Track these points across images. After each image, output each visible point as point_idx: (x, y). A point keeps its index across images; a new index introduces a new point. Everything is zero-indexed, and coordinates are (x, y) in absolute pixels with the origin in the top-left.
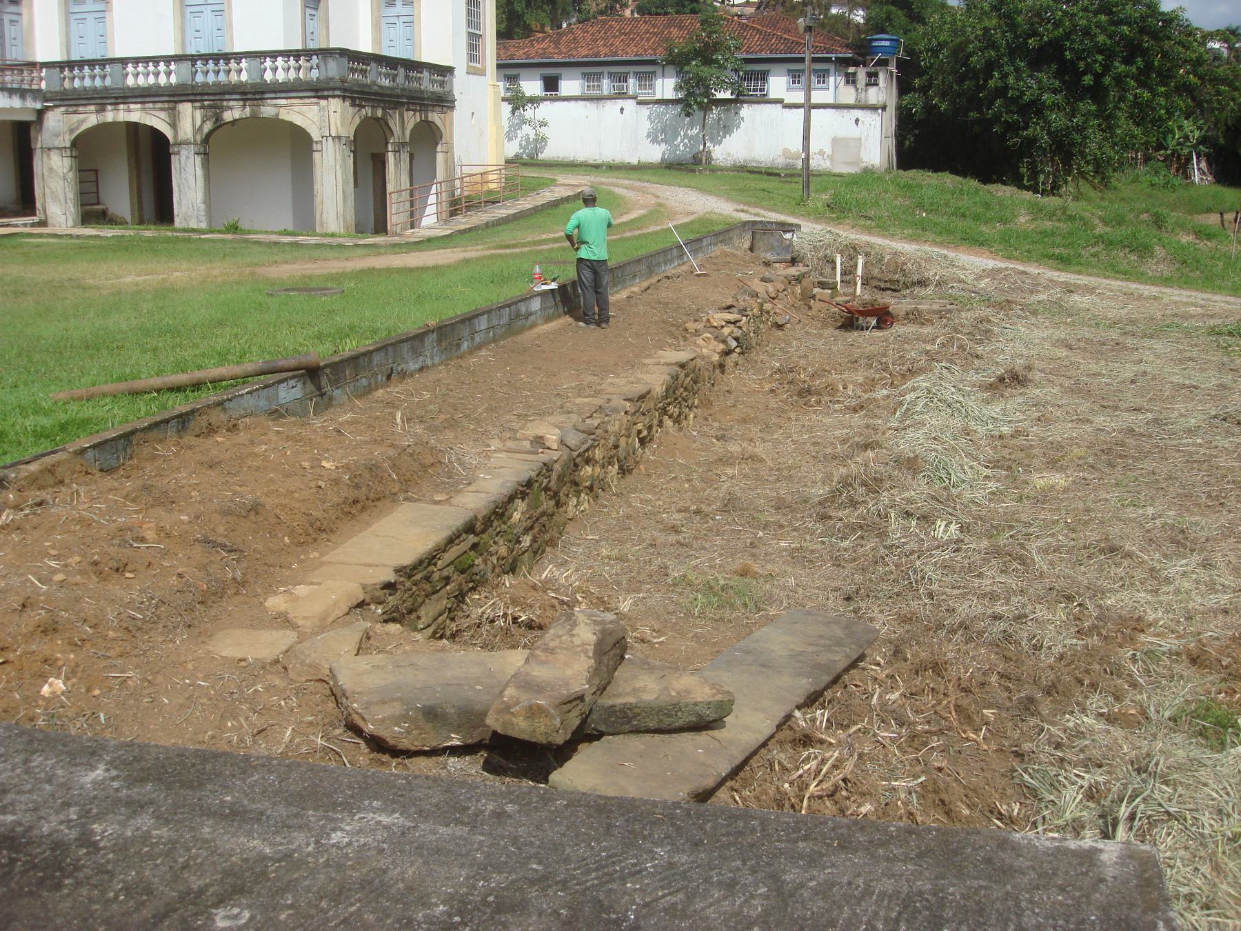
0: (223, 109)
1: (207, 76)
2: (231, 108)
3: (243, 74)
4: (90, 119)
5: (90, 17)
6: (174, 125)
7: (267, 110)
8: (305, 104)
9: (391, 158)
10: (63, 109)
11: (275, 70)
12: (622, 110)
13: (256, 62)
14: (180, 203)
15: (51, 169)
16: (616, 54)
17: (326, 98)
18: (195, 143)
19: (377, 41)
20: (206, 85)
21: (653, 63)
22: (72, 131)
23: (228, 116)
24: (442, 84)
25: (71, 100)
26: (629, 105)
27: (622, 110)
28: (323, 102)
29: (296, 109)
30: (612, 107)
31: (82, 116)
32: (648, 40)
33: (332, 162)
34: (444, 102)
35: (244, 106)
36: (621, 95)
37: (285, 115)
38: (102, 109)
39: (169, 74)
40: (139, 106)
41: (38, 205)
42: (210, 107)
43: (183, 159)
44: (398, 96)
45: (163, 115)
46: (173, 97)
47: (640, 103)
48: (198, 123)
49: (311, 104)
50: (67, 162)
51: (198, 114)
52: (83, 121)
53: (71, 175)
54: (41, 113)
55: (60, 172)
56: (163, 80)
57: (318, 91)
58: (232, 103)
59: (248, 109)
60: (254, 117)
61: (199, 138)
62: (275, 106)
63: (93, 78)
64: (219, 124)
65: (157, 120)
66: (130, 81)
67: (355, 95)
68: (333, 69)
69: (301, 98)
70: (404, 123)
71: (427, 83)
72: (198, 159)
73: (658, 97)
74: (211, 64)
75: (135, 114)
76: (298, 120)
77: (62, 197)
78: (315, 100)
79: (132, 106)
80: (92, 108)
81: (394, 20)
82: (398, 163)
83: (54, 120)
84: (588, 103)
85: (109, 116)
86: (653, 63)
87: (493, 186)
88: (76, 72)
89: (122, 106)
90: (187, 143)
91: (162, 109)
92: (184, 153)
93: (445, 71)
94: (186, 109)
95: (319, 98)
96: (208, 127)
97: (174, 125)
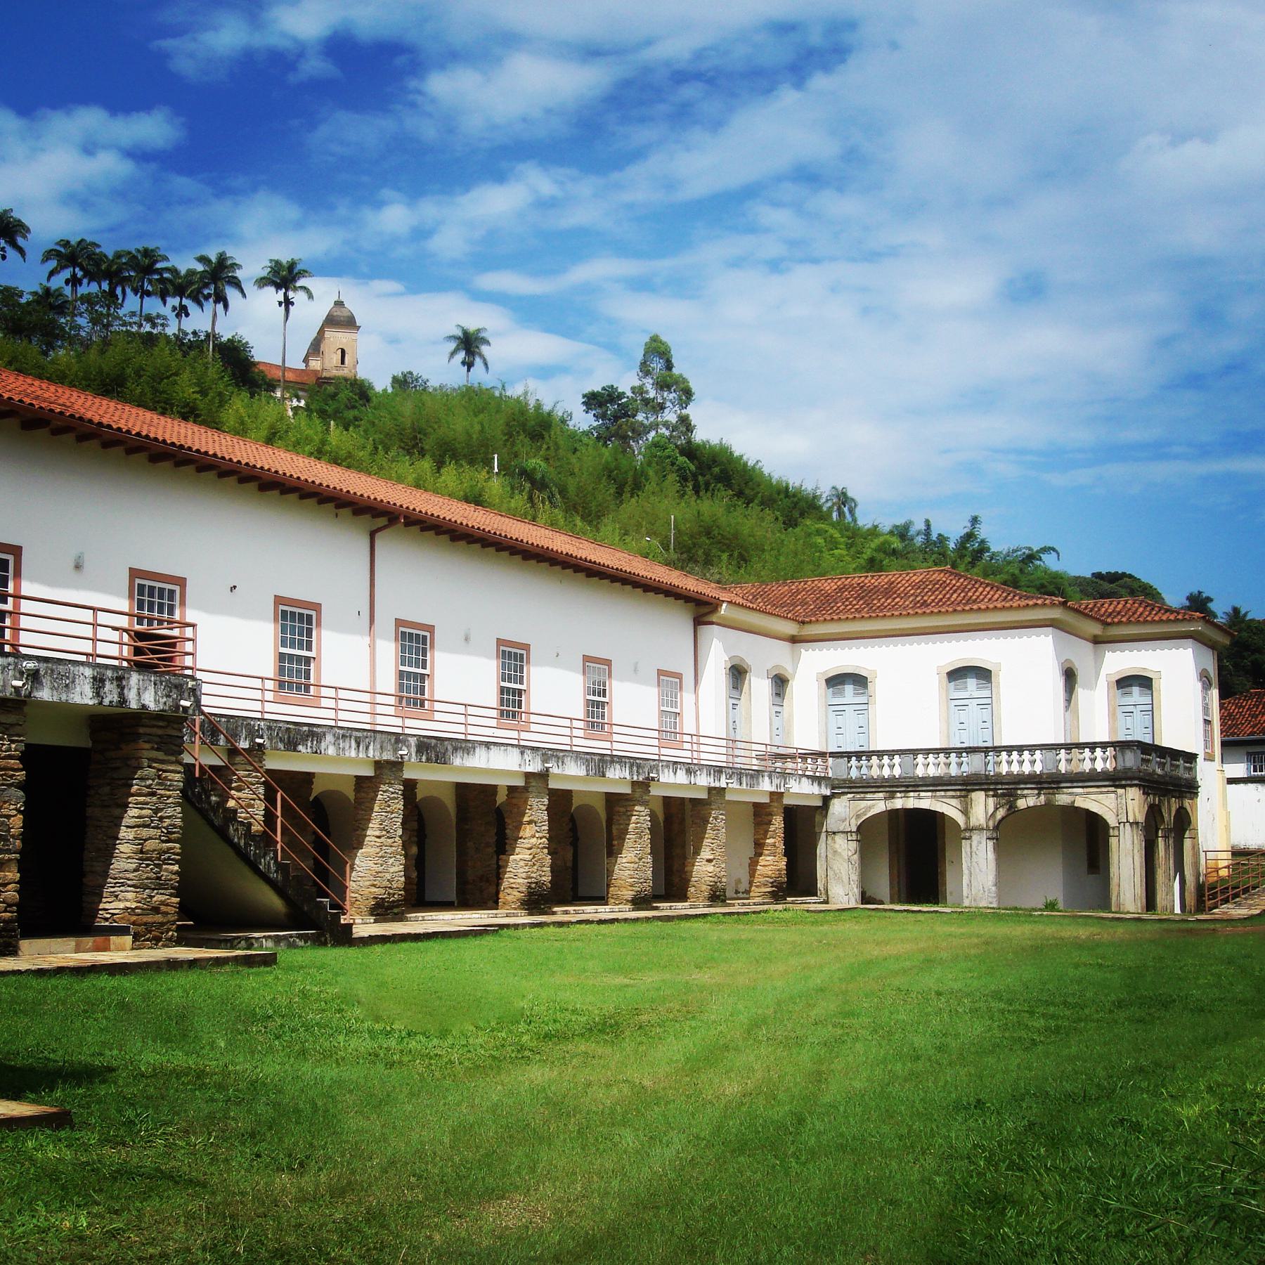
0: (1017, 797)
3: (1034, 765)
4: (878, 805)
6: (965, 812)
7: (1063, 799)
8: (1101, 793)
14: (970, 885)
18: (988, 829)
20: (1009, 774)
22: (858, 816)
23: (1022, 804)
28: (1120, 791)
29: (1093, 797)
34: (1190, 788)
35: (1039, 794)
37: (1081, 803)
38: (891, 796)
42: (1003, 795)
43: (974, 843)
45: (954, 802)
46: (966, 786)
48: (991, 810)
49: (1108, 792)
50: (853, 845)
52: (870, 807)
53: (856, 857)
54: (826, 800)
57: (1115, 780)
59: (1042, 797)
60: (1049, 804)
61: (991, 824)
62: (1071, 794)
65: (947, 806)
67: (1149, 785)
72: (990, 843)
75: (925, 802)
76: (1094, 808)
77: (846, 881)
80: (881, 795)
84: (1251, 786)
90: (980, 829)
91: (953, 797)
92: (976, 837)
94: (979, 797)
95: (1117, 787)
96: (1001, 813)
97: (965, 812)
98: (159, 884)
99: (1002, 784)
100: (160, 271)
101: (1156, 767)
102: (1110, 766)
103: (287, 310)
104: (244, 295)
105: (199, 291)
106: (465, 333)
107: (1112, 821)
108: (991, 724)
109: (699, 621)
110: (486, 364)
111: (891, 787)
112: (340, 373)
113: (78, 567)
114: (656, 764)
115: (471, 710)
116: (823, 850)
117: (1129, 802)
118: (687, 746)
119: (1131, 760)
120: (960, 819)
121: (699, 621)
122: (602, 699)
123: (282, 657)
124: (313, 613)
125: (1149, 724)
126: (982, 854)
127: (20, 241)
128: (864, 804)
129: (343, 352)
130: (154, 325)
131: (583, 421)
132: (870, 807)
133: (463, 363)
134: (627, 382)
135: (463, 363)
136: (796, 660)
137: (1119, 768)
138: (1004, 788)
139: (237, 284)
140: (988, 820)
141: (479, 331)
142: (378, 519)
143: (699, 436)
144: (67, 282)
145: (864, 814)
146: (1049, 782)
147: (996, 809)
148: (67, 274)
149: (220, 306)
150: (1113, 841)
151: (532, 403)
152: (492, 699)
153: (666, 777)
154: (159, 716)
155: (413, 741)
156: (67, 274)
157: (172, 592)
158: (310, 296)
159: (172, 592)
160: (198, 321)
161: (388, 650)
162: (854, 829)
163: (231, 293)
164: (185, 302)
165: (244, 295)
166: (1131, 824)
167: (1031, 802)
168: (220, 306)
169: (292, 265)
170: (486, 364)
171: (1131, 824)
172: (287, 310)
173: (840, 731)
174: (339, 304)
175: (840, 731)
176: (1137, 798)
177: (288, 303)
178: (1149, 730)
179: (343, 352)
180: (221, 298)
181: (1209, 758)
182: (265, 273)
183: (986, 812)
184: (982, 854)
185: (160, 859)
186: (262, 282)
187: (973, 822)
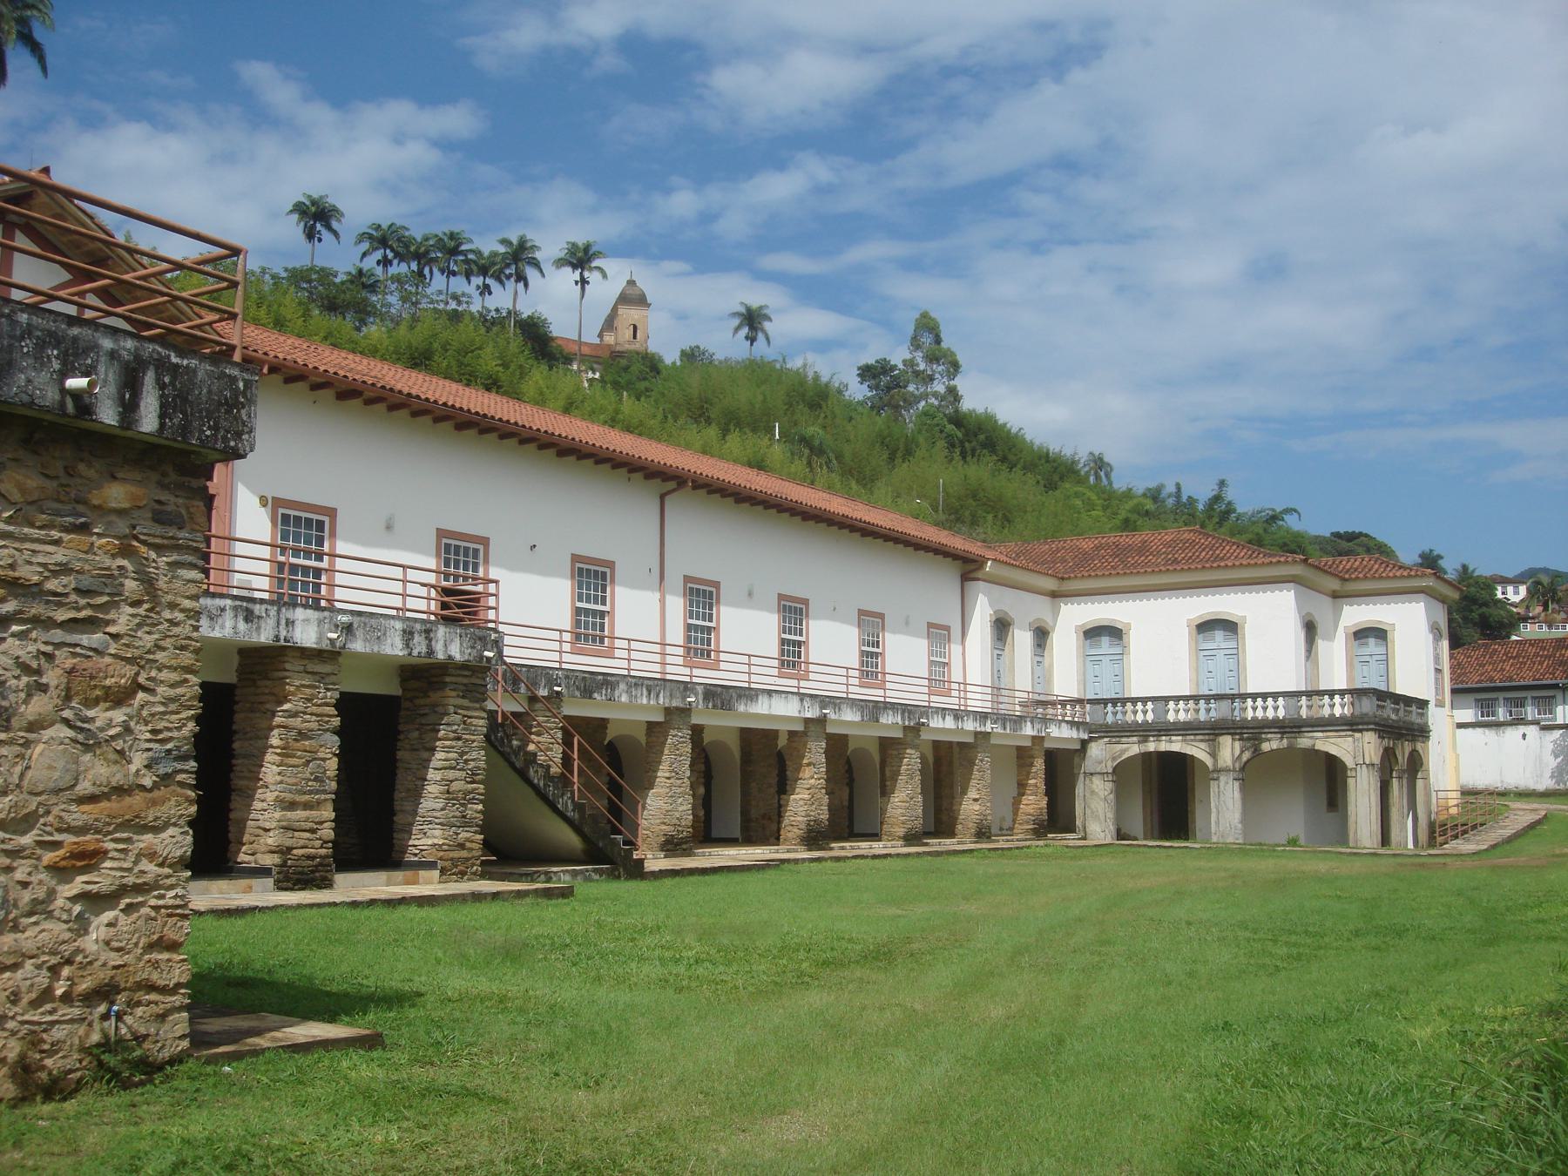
0: (1263, 741)
4: (1133, 748)
7: (1304, 742)
9: (1395, 782)
12: (1524, 736)
13: (1293, 701)
14: (1218, 823)
15: (1093, 792)
16: (1511, 679)
17: (1360, 731)
19: (1350, 678)
20: (1254, 719)
21: (1555, 687)
22: (1114, 759)
23: (1266, 747)
24: (1422, 715)
26: (1532, 731)
27: (1524, 736)
28: (1357, 735)
30: (1513, 734)
32: (1541, 663)
33: (1365, 783)
34: (1422, 733)
36: (1519, 721)
37: (1322, 746)
38: (1145, 740)
41: (1078, 823)
44: (1400, 728)
45: (1203, 745)
46: (1213, 731)
47: (1544, 728)
48: (1237, 752)
50: (1110, 785)
54: (1084, 743)
55: (1102, 794)
57: (1352, 725)
60: (1290, 748)
61: (1237, 766)
63: (1187, 711)
64: (1257, 752)
65: (1197, 750)
66: (1171, 717)
68: (1368, 706)
70: (1403, 750)
72: (1237, 784)
73: (1560, 721)
74: (1259, 701)
75: (1176, 745)
76: (1333, 751)
82: (1401, 787)
83: (1096, 750)
84: (1479, 730)
85: (1151, 746)
86: (1555, 687)
87: (1454, 811)
88: (1119, 708)
90: (1227, 770)
92: (1223, 779)
93: (1423, 704)
96: (1246, 756)
98: (465, 822)
100: (464, 253)
101: (1390, 713)
103: (583, 289)
105: (501, 271)
106: (749, 310)
107: (1349, 763)
109: (966, 578)
110: (768, 339)
112: (632, 347)
114: (926, 711)
115: (634, 645)
120: (1208, 761)
121: (966, 578)
124: (326, 519)
125: (1383, 672)
127: (335, 224)
129: (635, 328)
130: (459, 303)
131: (858, 391)
133: (747, 338)
134: (898, 356)
135: (747, 338)
136: (1056, 613)
138: (1251, 732)
139: (536, 264)
140: (1234, 762)
141: (761, 308)
142: (668, 482)
143: (967, 405)
144: (379, 263)
148: (378, 255)
149: (521, 285)
151: (811, 375)
153: (936, 723)
154: (464, 666)
155: (700, 689)
156: (378, 255)
157: (604, 574)
158: (605, 276)
159: (476, 551)
160: (501, 298)
161: (676, 605)
163: (531, 273)
164: (488, 281)
167: (1275, 745)
168: (521, 285)
169: (587, 248)
170: (768, 339)
172: (583, 289)
174: (631, 283)
177: (583, 282)
179: (635, 328)
180: (521, 278)
181: (1440, 704)
182: (562, 254)
185: (465, 799)
186: (560, 263)
187: (1221, 764)
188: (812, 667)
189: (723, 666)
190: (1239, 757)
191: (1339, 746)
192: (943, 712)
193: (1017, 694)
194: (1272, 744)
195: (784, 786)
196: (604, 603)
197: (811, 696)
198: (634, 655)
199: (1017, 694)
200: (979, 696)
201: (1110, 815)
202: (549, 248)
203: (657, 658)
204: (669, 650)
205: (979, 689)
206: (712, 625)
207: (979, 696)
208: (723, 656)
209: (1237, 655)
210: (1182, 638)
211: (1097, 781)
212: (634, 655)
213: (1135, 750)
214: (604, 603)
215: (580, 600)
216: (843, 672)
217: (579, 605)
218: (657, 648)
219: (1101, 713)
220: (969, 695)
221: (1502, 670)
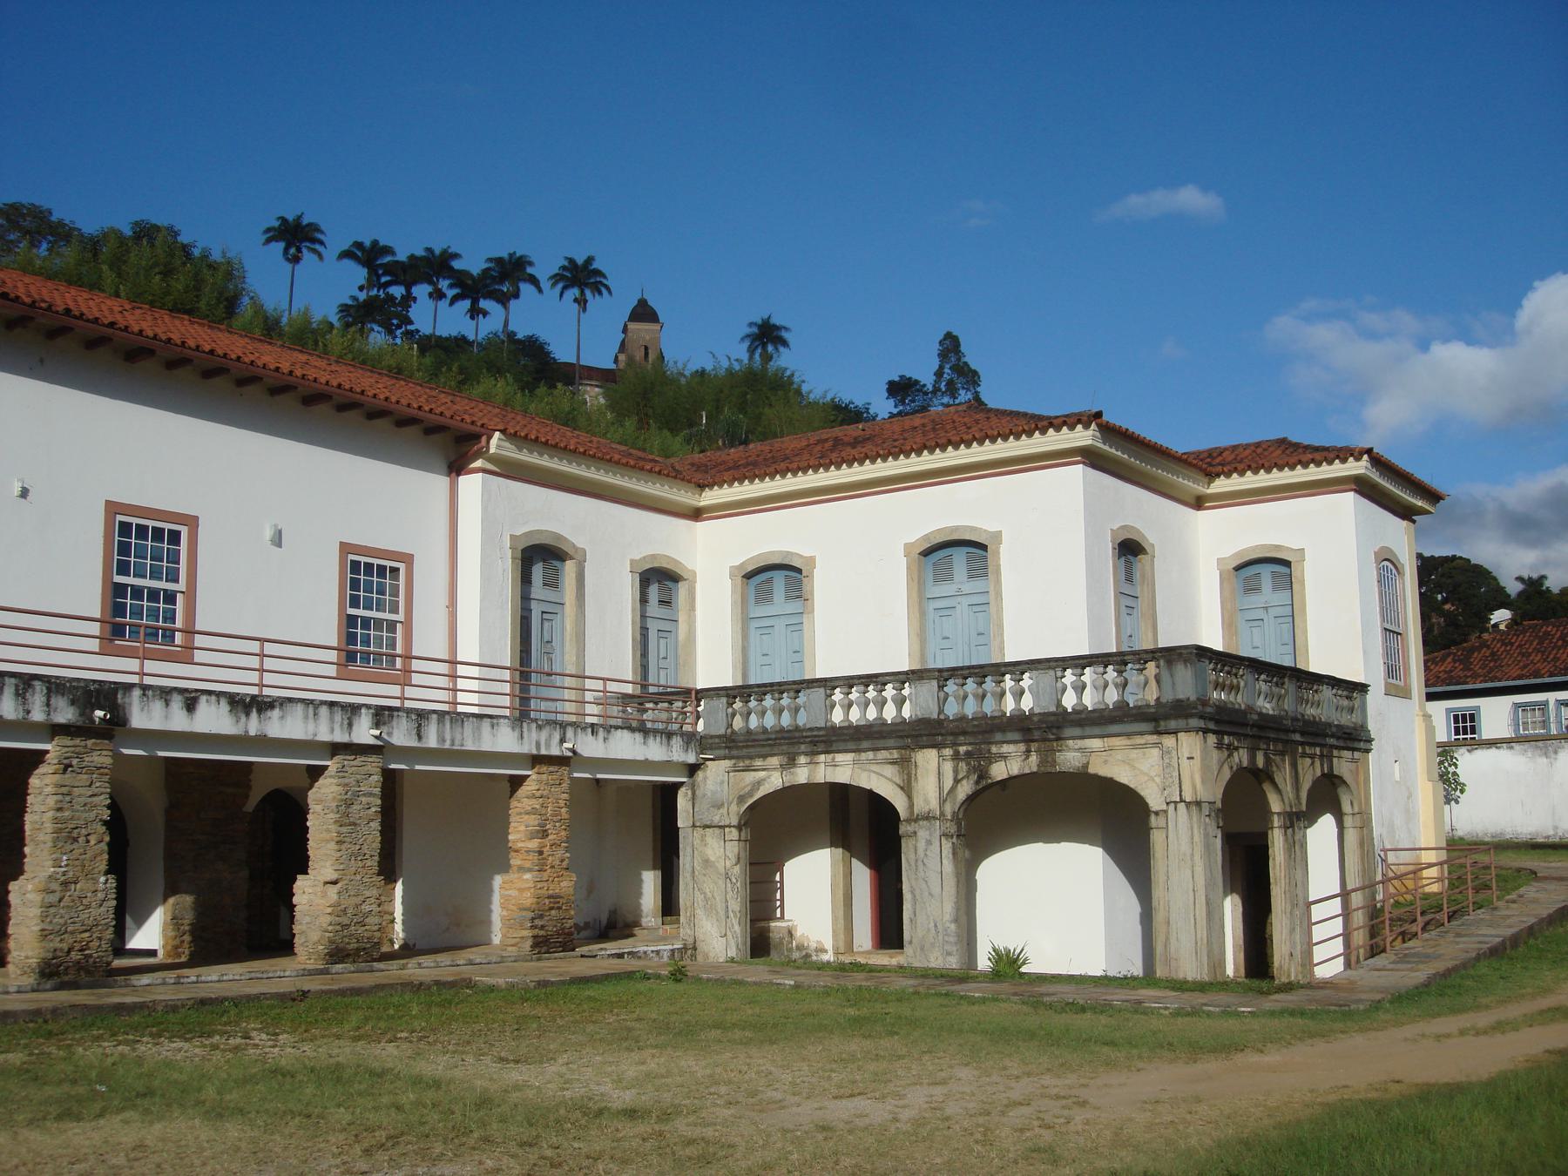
0: (992, 759)
1: (963, 703)
2: (1004, 757)
3: (1022, 698)
4: (771, 778)
5: (780, 624)
6: (907, 789)
7: (1070, 756)
8: (1135, 747)
10: (727, 763)
11: (1080, 688)
20: (962, 718)
22: (741, 799)
23: (999, 771)
25: (740, 747)
28: (1169, 741)
29: (1119, 756)
31: (762, 774)
33: (1185, 847)
34: (1356, 739)
39: (900, 702)
40: (850, 757)
43: (921, 845)
45: (890, 771)
46: (909, 737)
48: (948, 783)
49: (1144, 746)
50: (733, 849)
51: (948, 767)
52: (759, 783)
53: (737, 869)
56: (890, 713)
57: (1158, 719)
58: (1006, 748)
59: (1034, 758)
67: (1226, 724)
69: (1129, 735)
71: (1325, 708)
75: (842, 769)
76: (1123, 776)
77: (720, 907)
78: (1154, 738)
79: (840, 757)
81: (1260, 614)
85: (802, 775)
89: (822, 758)
90: (928, 817)
93: (1362, 688)
94: (928, 760)
95: (1159, 733)
96: (965, 789)
97: (907, 789)
99: (964, 733)
101: (1262, 700)
102: (1151, 695)
104: (540, 291)
107: (1155, 801)
108: (989, 630)
111: (790, 743)
113: (278, 540)
115: (269, 648)
116: (689, 859)
117: (1185, 763)
118: (567, 694)
119: (1184, 685)
122: (171, 586)
123: (351, 621)
125: (1288, 638)
126: (933, 863)
128: (750, 777)
129: (646, 348)
132: (759, 783)
134: (924, 371)
137: (1163, 700)
138: (971, 737)
140: (942, 802)
145: (750, 794)
146: (1047, 728)
147: (957, 781)
150: (1157, 837)
151: (788, 373)
152: (330, 634)
153: (145, 716)
157: (395, 570)
159: (395, 570)
162: (735, 822)
165: (540, 291)
166: (1188, 804)
171: (1188, 804)
173: (766, 660)
175: (766, 660)
176: (1197, 754)
178: (1290, 648)
179: (646, 348)
181: (1397, 690)
183: (940, 788)
184: (933, 863)
187: (920, 806)
188: (416, 665)
189: (199, 656)
190: (953, 790)
191: (1136, 764)
192: (165, 694)
193: (589, 684)
194: (1011, 762)
195: (292, 857)
196: (395, 610)
197: (332, 704)
198: (269, 664)
199: (589, 684)
200: (475, 685)
201: (736, 905)
202: (544, 268)
203: (443, 682)
204: (461, 670)
205: (475, 672)
206: (400, 617)
207: (475, 685)
208: (199, 640)
209: (986, 606)
210: (894, 579)
211: (712, 838)
212: (269, 664)
213: (774, 780)
214: (395, 610)
215: (355, 602)
216: (254, 647)
217: (351, 611)
218: (443, 668)
219: (721, 716)
220: (461, 684)
221: (1556, 659)
